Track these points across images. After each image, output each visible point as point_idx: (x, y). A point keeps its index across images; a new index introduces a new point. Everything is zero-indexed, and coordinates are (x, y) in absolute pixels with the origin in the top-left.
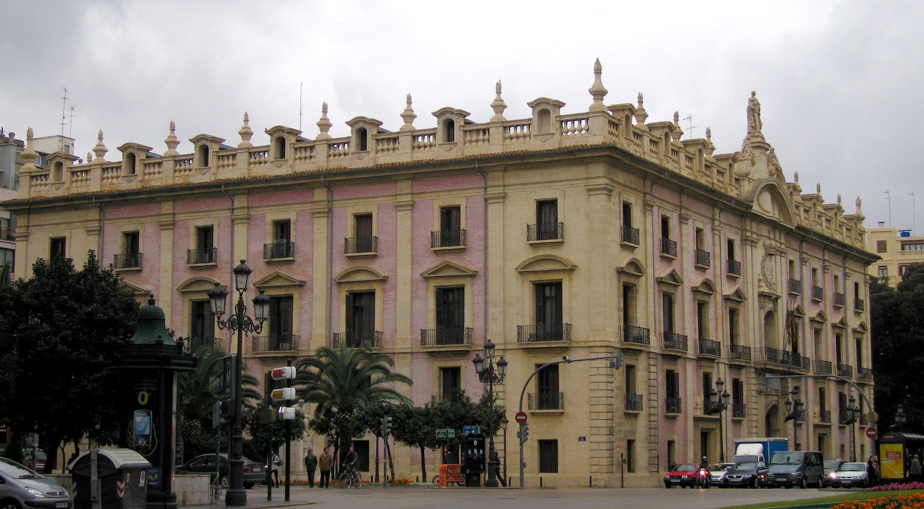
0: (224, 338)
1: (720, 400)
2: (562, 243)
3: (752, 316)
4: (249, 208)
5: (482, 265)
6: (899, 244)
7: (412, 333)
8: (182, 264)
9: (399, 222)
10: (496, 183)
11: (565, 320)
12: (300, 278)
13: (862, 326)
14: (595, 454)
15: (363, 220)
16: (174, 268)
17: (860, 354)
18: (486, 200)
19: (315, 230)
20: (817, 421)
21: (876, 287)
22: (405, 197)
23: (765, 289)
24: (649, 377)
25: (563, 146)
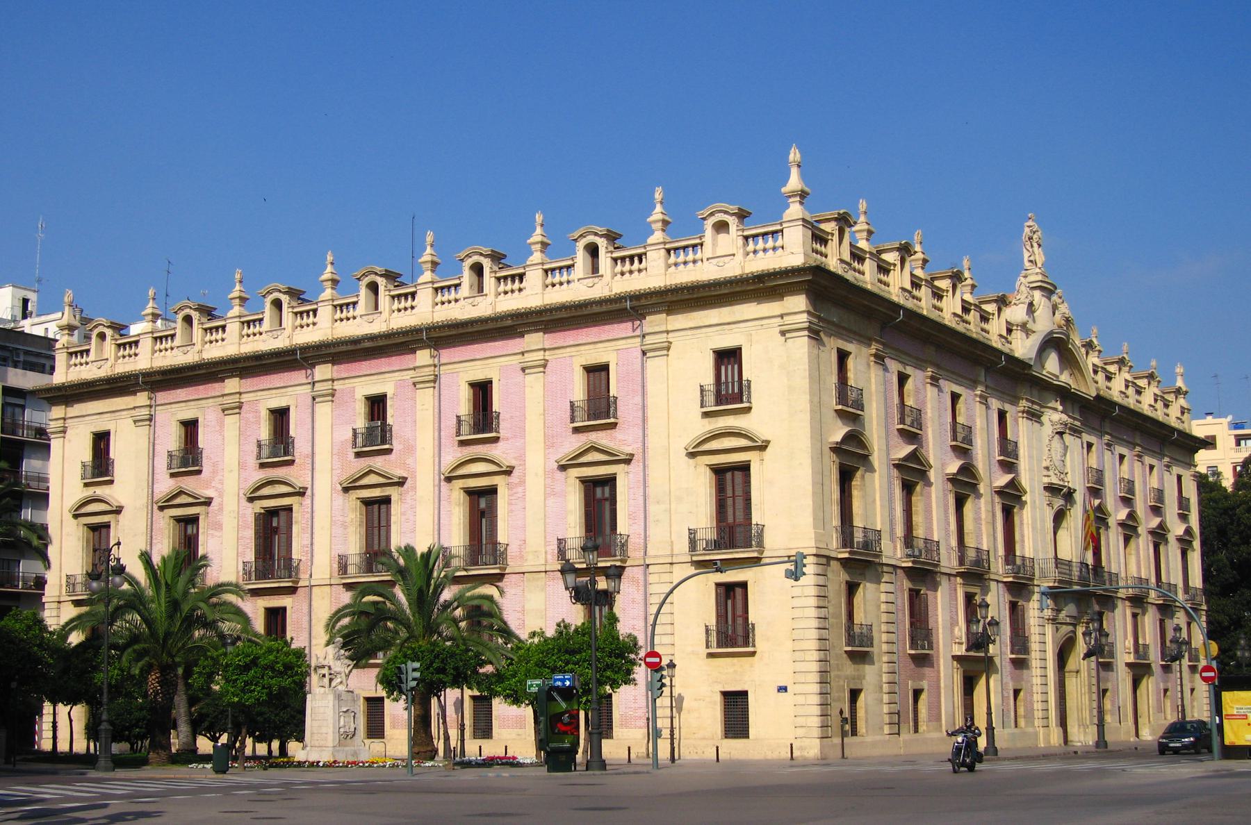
0: (303, 559)
1: (985, 628)
2: (749, 409)
3: (1034, 516)
4: (333, 380)
5: (640, 445)
6: (1233, 441)
7: (546, 544)
8: (252, 462)
9: (527, 390)
10: (657, 329)
11: (755, 519)
12: (399, 472)
13: (1188, 531)
14: (801, 711)
15: (482, 390)
16: (242, 466)
17: (1186, 571)
18: (644, 353)
19: (419, 407)
20: (1131, 659)
21: (1207, 485)
22: (535, 354)
23: (1055, 480)
24: (879, 603)
25: (747, 271)
